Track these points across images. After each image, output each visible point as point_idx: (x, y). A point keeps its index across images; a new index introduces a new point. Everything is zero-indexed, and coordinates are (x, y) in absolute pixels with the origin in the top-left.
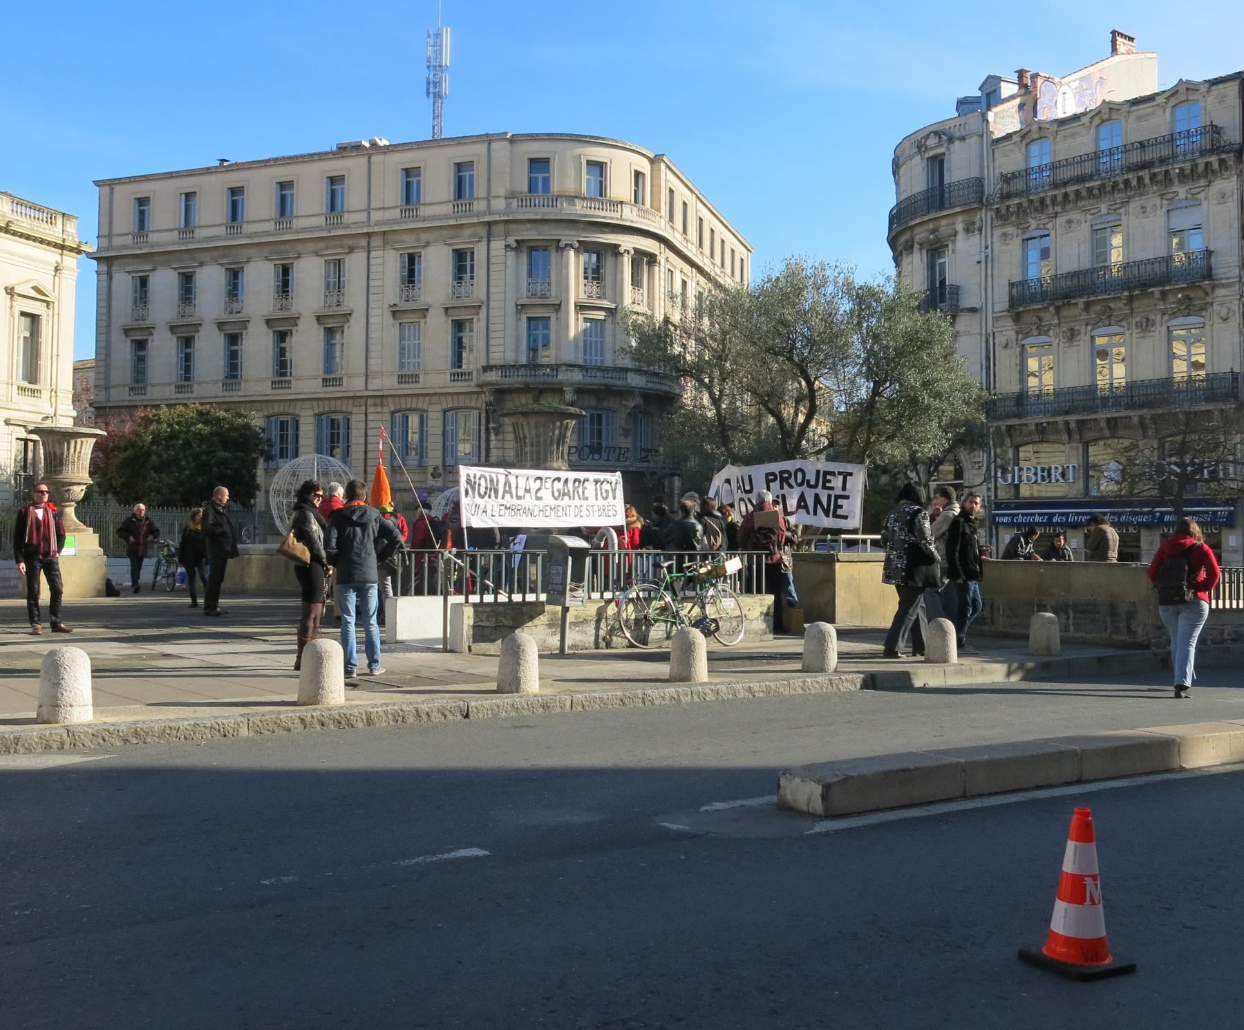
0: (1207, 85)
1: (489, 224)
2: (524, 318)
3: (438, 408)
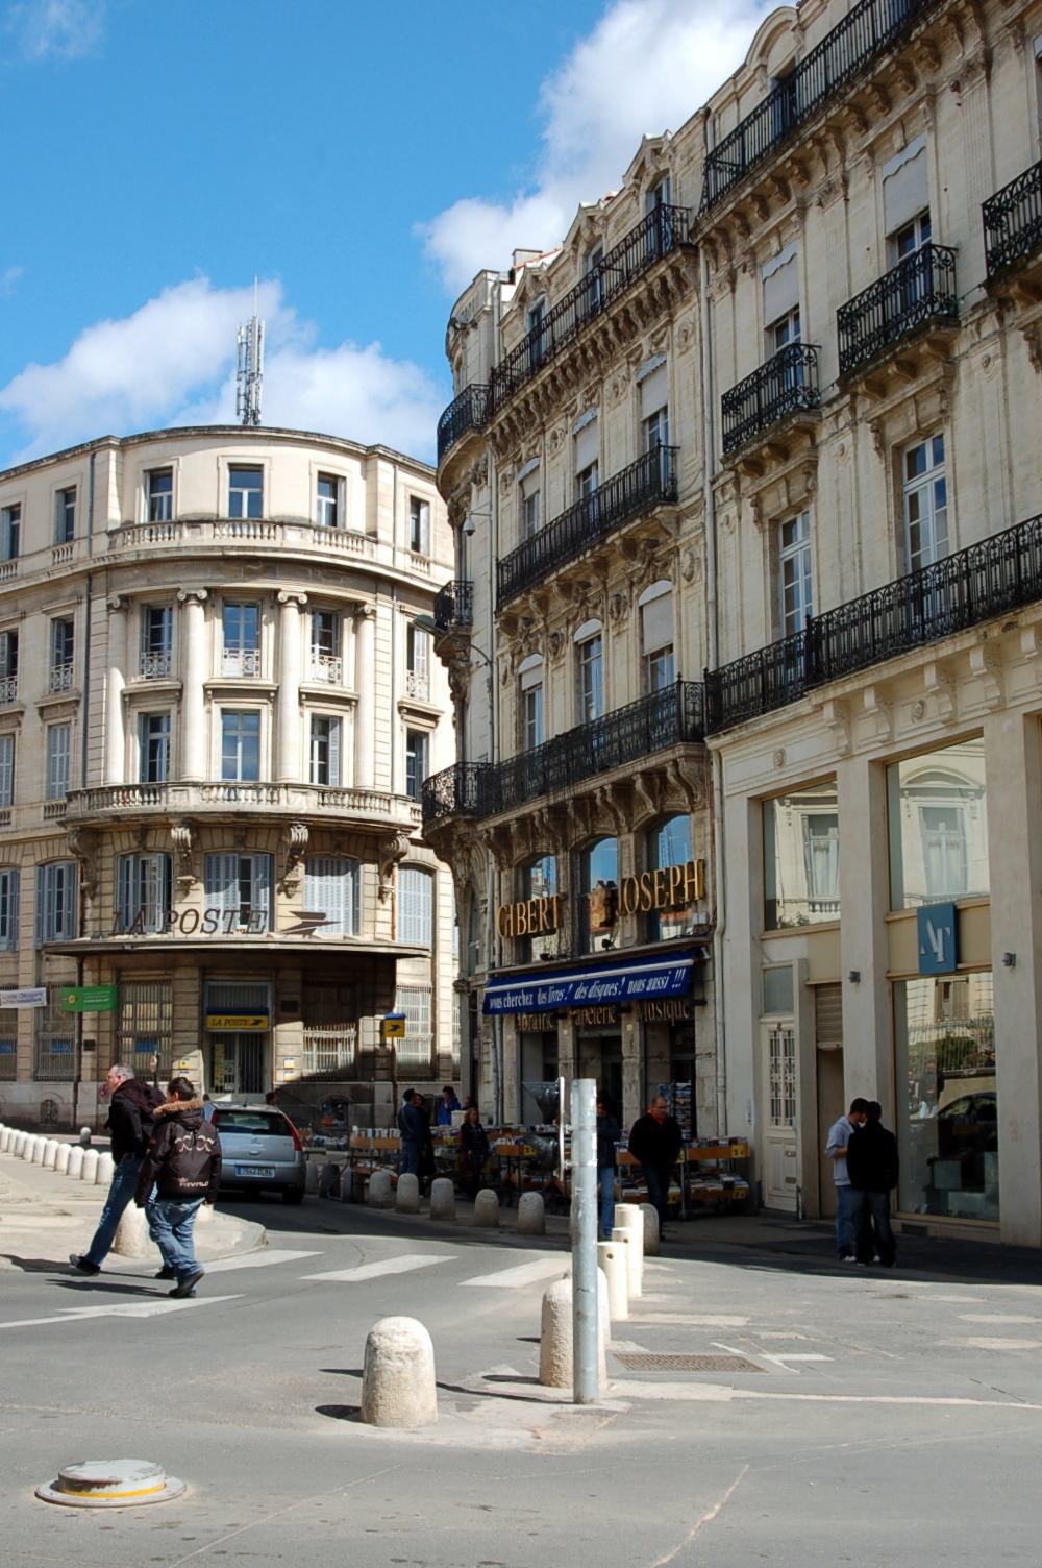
0: (610, 1171)
1: (89, 575)
2: (134, 714)
3: (30, 861)
